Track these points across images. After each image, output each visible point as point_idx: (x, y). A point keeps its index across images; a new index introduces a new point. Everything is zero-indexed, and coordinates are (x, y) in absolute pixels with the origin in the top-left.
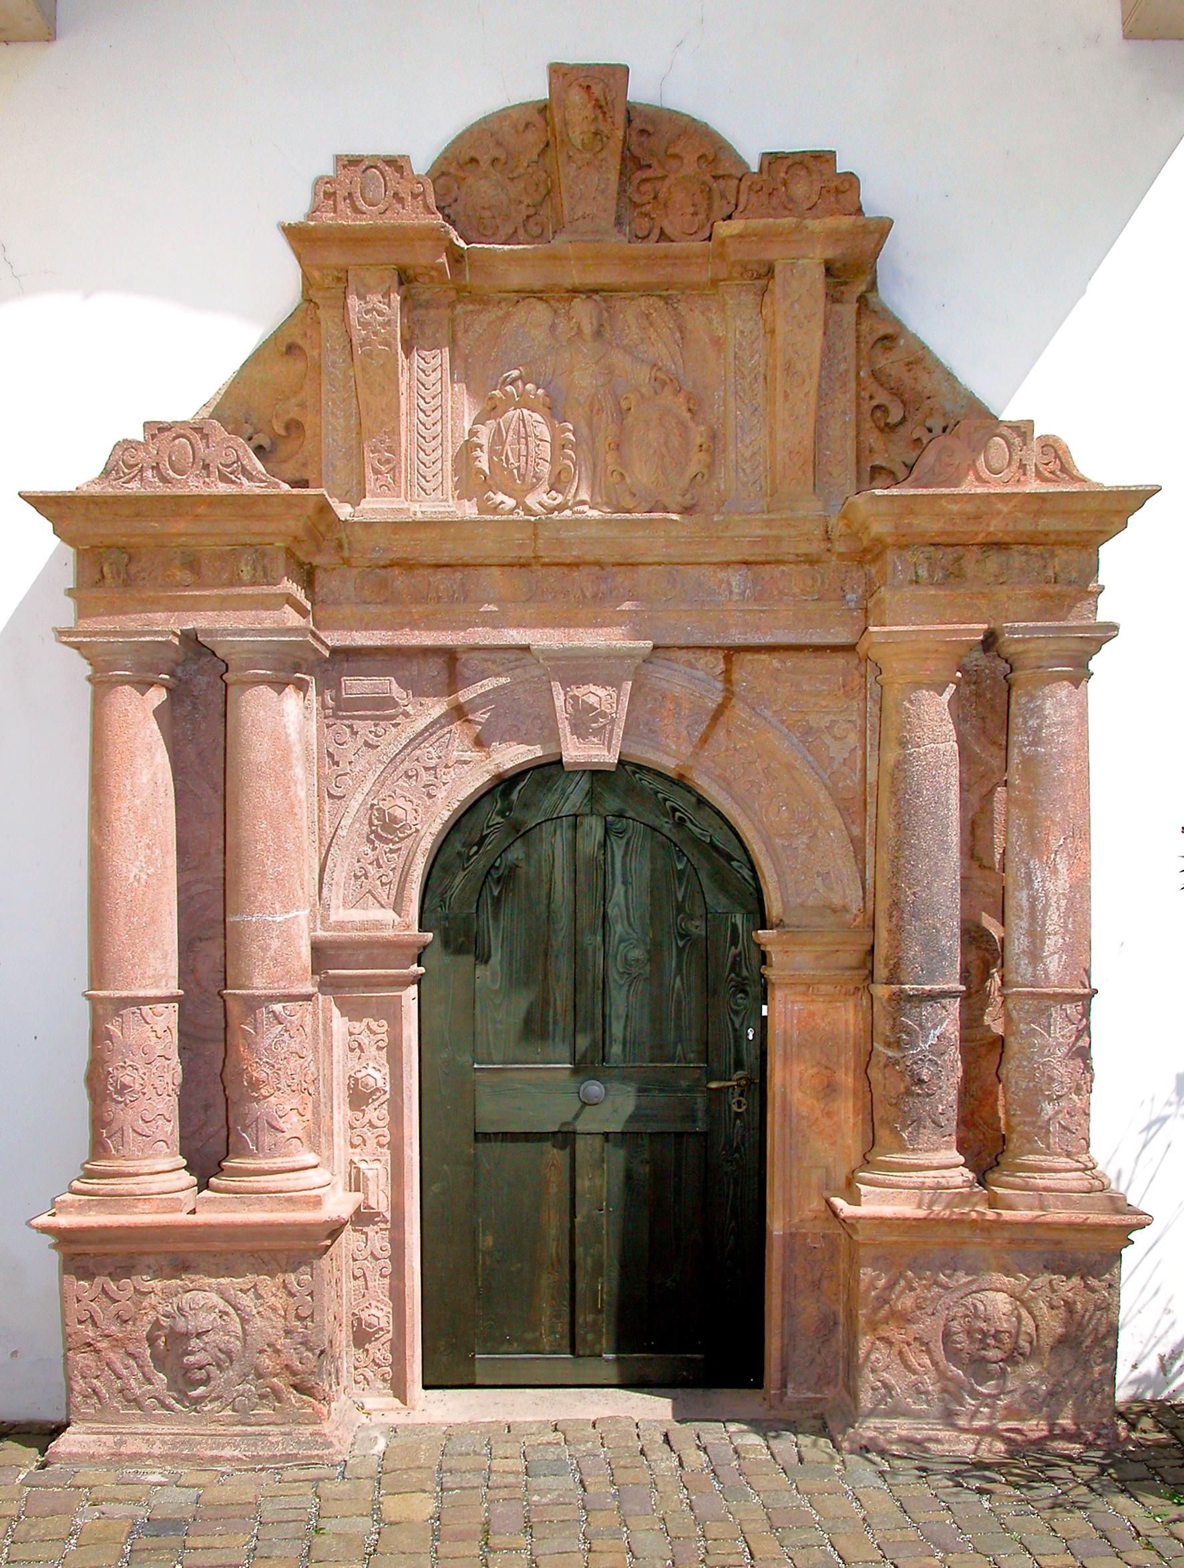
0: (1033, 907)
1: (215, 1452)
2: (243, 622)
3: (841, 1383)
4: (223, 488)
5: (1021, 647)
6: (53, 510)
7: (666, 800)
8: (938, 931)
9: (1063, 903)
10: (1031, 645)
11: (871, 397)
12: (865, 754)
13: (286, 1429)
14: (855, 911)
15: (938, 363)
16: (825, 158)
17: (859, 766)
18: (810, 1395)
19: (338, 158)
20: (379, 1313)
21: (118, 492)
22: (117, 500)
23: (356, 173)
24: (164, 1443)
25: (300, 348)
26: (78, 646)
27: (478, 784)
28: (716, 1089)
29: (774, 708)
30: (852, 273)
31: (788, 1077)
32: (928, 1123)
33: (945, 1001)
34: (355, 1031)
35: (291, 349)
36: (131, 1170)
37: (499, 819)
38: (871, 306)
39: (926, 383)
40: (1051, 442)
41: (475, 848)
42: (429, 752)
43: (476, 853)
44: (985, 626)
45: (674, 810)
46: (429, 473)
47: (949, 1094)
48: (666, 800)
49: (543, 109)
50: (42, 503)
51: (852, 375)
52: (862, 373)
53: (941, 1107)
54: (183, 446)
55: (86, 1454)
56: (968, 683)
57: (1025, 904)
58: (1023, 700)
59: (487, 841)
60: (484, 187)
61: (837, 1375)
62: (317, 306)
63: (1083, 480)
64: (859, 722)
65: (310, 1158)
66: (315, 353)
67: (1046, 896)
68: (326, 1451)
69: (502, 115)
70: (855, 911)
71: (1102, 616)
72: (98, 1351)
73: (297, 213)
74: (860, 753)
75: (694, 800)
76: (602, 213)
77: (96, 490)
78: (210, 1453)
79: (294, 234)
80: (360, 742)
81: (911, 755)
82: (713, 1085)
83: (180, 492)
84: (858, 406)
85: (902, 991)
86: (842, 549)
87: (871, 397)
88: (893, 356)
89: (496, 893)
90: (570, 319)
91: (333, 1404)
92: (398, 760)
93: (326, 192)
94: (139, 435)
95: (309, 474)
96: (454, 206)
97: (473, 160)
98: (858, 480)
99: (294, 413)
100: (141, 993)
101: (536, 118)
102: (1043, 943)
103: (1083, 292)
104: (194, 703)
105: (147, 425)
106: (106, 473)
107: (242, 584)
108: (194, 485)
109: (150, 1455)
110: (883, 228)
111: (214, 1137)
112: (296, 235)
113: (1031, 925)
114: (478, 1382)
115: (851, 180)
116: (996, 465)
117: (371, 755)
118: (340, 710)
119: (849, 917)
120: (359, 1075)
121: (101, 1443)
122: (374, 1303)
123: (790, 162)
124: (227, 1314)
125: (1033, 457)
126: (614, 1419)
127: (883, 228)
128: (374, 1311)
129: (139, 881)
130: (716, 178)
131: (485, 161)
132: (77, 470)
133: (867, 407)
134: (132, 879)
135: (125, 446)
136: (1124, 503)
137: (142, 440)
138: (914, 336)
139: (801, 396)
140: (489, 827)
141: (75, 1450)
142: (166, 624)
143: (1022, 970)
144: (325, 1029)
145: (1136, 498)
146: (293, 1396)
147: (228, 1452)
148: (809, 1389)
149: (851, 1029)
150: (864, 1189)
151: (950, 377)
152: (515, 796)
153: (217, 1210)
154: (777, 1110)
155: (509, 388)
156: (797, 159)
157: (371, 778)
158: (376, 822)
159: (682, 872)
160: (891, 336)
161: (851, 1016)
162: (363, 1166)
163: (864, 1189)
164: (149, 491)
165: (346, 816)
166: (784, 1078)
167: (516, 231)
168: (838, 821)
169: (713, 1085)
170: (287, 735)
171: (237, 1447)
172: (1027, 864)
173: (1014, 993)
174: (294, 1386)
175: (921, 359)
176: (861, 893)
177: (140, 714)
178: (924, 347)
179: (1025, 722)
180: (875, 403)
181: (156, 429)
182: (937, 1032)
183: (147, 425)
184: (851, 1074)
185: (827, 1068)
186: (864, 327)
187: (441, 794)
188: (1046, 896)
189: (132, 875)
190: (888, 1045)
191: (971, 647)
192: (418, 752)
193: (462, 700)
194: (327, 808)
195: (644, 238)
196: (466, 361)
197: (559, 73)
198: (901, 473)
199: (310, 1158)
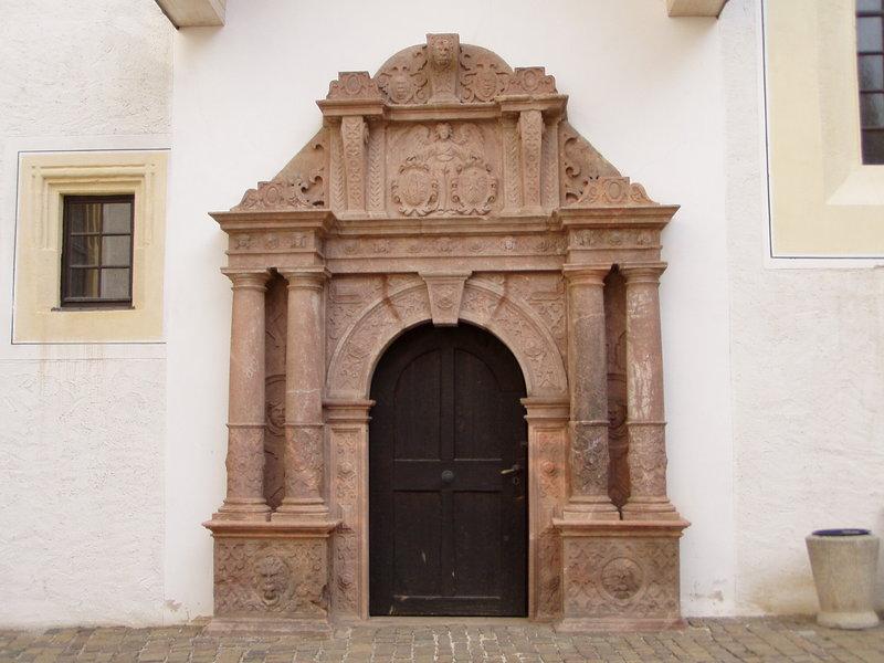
2: (298, 262)
4: (290, 209)
16: (541, 70)
23: (346, 79)
26: (227, 275)
30: (555, 113)
39: (589, 158)
42: (374, 319)
49: (425, 47)
50: (217, 216)
60: (399, 79)
65: (320, 500)
73: (323, 97)
76: (445, 95)
77: (238, 211)
79: (322, 105)
82: (504, 472)
85: (580, 424)
93: (334, 86)
95: (323, 199)
97: (395, 68)
103: (227, 462)
106: (244, 201)
109: (249, 632)
111: (273, 490)
115: (551, 78)
121: (227, 626)
125: (630, 192)
127: (564, 100)
131: (400, 68)
132: (230, 202)
133: (564, 168)
135: (250, 192)
147: (283, 630)
153: (277, 522)
165: (346, 348)
168: (555, 348)
169: (504, 472)
174: (313, 602)
177: (254, 304)
181: (262, 185)
186: (562, 135)
187: (380, 337)
190: (576, 449)
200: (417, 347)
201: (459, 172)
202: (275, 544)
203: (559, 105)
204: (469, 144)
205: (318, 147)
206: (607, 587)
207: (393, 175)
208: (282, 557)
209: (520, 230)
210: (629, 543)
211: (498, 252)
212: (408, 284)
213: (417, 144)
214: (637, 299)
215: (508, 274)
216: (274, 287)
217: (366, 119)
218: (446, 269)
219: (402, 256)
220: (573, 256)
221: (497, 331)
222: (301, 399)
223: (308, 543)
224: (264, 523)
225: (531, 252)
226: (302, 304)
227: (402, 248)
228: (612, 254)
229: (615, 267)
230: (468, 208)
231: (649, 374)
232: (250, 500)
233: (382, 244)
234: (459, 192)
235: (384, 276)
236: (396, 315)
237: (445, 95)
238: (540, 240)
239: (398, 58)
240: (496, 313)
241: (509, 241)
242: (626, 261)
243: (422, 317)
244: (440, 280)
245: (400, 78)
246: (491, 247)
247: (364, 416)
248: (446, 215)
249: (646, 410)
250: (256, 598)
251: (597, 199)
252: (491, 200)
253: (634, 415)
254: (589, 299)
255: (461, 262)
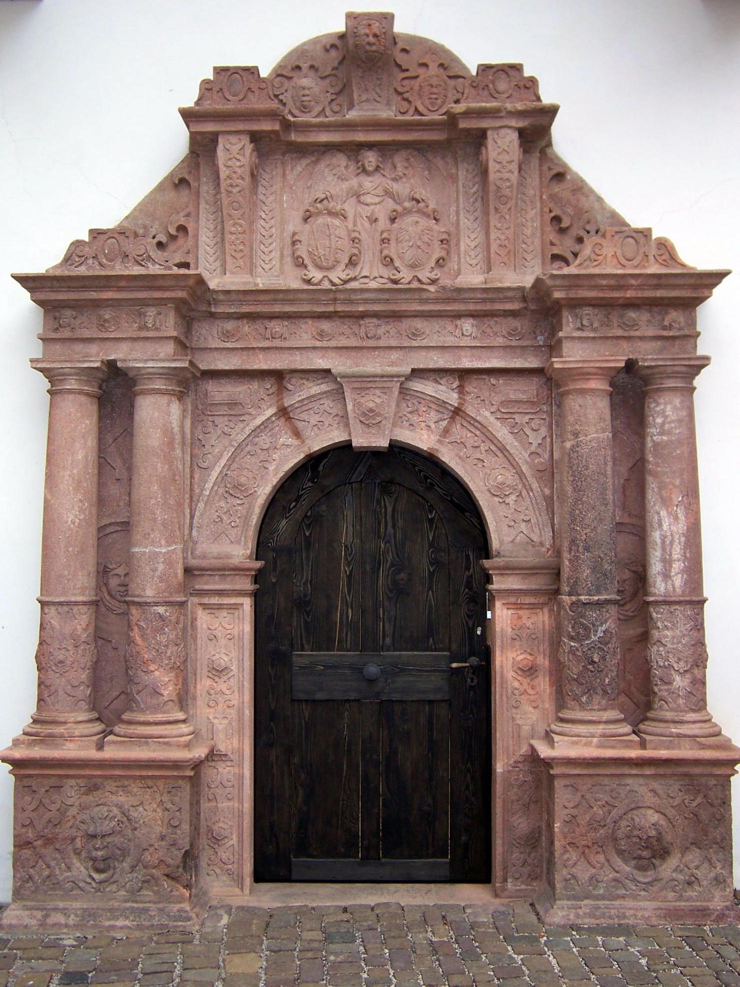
0: (663, 542)
1: (111, 923)
2: (149, 354)
3: (544, 878)
4: (137, 270)
5: (649, 371)
6: (31, 284)
7: (420, 471)
8: (602, 560)
9: (683, 539)
10: (656, 370)
11: (551, 211)
12: (552, 440)
13: (161, 906)
14: (548, 546)
15: (592, 191)
16: (517, 68)
17: (548, 449)
18: (523, 887)
19: (215, 68)
20: (225, 826)
21: (72, 274)
22: (70, 278)
23: (224, 77)
24: (76, 915)
25: (189, 184)
27: (296, 461)
28: (456, 668)
29: (492, 410)
30: (536, 127)
31: (505, 661)
32: (599, 691)
33: (609, 607)
34: (212, 628)
35: (183, 182)
36: (63, 720)
37: (310, 484)
38: (549, 155)
39: (584, 203)
40: (663, 242)
41: (294, 504)
42: (264, 440)
43: (294, 507)
44: (626, 358)
45: (426, 478)
46: (267, 259)
47: (612, 671)
48: (420, 471)
49: (342, 37)
50: (25, 280)
51: (538, 198)
52: (544, 197)
53: (607, 681)
54: (113, 244)
55: (21, 925)
56: (618, 394)
57: (658, 541)
58: (653, 405)
59: (303, 498)
61: (542, 872)
62: (198, 155)
63: (683, 266)
64: (548, 419)
65: (181, 716)
66: (196, 184)
67: (672, 535)
68: (189, 923)
69: (315, 41)
70: (548, 546)
71: (700, 352)
72: (35, 848)
74: (548, 440)
75: (439, 471)
77: (58, 273)
78: (107, 923)
80: (219, 432)
81: (581, 441)
82: (454, 665)
83: (109, 273)
84: (542, 216)
85: (579, 601)
86: (533, 308)
87: (551, 211)
88: (563, 186)
89: (307, 534)
90: (358, 162)
91: (193, 890)
92: (244, 444)
93: (206, 87)
94: (86, 238)
95: (190, 259)
96: (285, 94)
98: (543, 263)
99: (182, 221)
100: (73, 599)
101: (338, 42)
102: (671, 566)
104: (112, 407)
105: (91, 231)
107: (148, 329)
108: (119, 269)
110: (552, 111)
112: (187, 115)
113: (662, 555)
114: (293, 877)
115: (533, 81)
116: (629, 256)
117: (226, 441)
118: (201, 414)
119: (544, 549)
120: (214, 658)
121: (32, 917)
122: (222, 819)
123: (494, 70)
124: (122, 822)
126: (387, 904)
128: (221, 825)
129: (74, 523)
130: (449, 77)
132: (46, 259)
134: (69, 523)
135: (77, 244)
136: (711, 280)
137: (87, 239)
138: (576, 174)
139: (506, 210)
140: (303, 489)
141: (14, 922)
142: (95, 357)
143: (658, 585)
144: (192, 626)
145: (718, 277)
146: (166, 884)
147: (119, 923)
148: (522, 883)
149: (547, 627)
150: (556, 738)
151: (599, 199)
152: (321, 468)
153: (110, 753)
154: (498, 685)
155: (319, 205)
156: (499, 68)
157: (226, 456)
158: (228, 486)
159: (433, 519)
160: (560, 175)
161: (546, 618)
162: (216, 721)
163: (556, 738)
164: (91, 273)
166: (502, 661)
167: (324, 109)
169: (454, 665)
170: (172, 428)
171: (127, 918)
172: (659, 514)
173: (653, 602)
174: (167, 876)
175: (580, 188)
176: (551, 534)
177: (82, 417)
178: (583, 181)
179: (654, 420)
180: (553, 214)
181: (95, 234)
182: (604, 628)
183: (91, 231)
184: (547, 658)
185: (531, 654)
187: (272, 468)
188: (672, 535)
189: (70, 519)
190: (572, 638)
191: (619, 370)
192: (257, 439)
193: (286, 405)
194: (196, 476)
195: (404, 113)
196: (291, 188)
197: (350, 16)
198: (570, 257)
199: (181, 716)
200: (326, 474)
201: (393, 220)
202: (111, 785)
203: (542, 121)
204: (410, 181)
205: (183, 182)
206: (620, 853)
207: (294, 224)
208: (119, 807)
209: (485, 307)
210: (655, 785)
211: (450, 341)
212: (316, 388)
213: (332, 179)
214: (663, 411)
215: (464, 374)
216: (114, 392)
217: (255, 137)
218: (372, 365)
219: (305, 347)
220: (567, 347)
221: (447, 457)
222: (155, 557)
223: (161, 783)
224: (93, 754)
225: (500, 341)
226: (158, 416)
227: (305, 333)
228: (624, 344)
229: (630, 366)
230: (405, 275)
231: (681, 527)
232: (72, 717)
233: (276, 327)
234: (392, 250)
235: (278, 376)
236: (297, 434)
237: (373, 107)
238: (515, 323)
239: (300, 52)
240: (446, 432)
241: (467, 325)
242: (648, 355)
243: (336, 436)
244: (364, 382)
245: (306, 81)
246: (436, 333)
247: (248, 585)
248: (373, 285)
249: (678, 581)
250: (80, 869)
251: (604, 261)
252: (440, 263)
253: (659, 587)
254: (591, 415)
255: (394, 355)
